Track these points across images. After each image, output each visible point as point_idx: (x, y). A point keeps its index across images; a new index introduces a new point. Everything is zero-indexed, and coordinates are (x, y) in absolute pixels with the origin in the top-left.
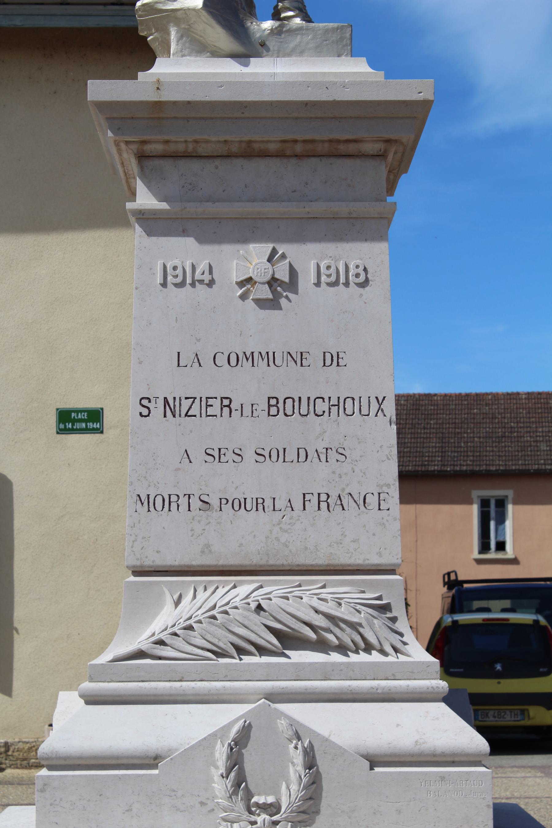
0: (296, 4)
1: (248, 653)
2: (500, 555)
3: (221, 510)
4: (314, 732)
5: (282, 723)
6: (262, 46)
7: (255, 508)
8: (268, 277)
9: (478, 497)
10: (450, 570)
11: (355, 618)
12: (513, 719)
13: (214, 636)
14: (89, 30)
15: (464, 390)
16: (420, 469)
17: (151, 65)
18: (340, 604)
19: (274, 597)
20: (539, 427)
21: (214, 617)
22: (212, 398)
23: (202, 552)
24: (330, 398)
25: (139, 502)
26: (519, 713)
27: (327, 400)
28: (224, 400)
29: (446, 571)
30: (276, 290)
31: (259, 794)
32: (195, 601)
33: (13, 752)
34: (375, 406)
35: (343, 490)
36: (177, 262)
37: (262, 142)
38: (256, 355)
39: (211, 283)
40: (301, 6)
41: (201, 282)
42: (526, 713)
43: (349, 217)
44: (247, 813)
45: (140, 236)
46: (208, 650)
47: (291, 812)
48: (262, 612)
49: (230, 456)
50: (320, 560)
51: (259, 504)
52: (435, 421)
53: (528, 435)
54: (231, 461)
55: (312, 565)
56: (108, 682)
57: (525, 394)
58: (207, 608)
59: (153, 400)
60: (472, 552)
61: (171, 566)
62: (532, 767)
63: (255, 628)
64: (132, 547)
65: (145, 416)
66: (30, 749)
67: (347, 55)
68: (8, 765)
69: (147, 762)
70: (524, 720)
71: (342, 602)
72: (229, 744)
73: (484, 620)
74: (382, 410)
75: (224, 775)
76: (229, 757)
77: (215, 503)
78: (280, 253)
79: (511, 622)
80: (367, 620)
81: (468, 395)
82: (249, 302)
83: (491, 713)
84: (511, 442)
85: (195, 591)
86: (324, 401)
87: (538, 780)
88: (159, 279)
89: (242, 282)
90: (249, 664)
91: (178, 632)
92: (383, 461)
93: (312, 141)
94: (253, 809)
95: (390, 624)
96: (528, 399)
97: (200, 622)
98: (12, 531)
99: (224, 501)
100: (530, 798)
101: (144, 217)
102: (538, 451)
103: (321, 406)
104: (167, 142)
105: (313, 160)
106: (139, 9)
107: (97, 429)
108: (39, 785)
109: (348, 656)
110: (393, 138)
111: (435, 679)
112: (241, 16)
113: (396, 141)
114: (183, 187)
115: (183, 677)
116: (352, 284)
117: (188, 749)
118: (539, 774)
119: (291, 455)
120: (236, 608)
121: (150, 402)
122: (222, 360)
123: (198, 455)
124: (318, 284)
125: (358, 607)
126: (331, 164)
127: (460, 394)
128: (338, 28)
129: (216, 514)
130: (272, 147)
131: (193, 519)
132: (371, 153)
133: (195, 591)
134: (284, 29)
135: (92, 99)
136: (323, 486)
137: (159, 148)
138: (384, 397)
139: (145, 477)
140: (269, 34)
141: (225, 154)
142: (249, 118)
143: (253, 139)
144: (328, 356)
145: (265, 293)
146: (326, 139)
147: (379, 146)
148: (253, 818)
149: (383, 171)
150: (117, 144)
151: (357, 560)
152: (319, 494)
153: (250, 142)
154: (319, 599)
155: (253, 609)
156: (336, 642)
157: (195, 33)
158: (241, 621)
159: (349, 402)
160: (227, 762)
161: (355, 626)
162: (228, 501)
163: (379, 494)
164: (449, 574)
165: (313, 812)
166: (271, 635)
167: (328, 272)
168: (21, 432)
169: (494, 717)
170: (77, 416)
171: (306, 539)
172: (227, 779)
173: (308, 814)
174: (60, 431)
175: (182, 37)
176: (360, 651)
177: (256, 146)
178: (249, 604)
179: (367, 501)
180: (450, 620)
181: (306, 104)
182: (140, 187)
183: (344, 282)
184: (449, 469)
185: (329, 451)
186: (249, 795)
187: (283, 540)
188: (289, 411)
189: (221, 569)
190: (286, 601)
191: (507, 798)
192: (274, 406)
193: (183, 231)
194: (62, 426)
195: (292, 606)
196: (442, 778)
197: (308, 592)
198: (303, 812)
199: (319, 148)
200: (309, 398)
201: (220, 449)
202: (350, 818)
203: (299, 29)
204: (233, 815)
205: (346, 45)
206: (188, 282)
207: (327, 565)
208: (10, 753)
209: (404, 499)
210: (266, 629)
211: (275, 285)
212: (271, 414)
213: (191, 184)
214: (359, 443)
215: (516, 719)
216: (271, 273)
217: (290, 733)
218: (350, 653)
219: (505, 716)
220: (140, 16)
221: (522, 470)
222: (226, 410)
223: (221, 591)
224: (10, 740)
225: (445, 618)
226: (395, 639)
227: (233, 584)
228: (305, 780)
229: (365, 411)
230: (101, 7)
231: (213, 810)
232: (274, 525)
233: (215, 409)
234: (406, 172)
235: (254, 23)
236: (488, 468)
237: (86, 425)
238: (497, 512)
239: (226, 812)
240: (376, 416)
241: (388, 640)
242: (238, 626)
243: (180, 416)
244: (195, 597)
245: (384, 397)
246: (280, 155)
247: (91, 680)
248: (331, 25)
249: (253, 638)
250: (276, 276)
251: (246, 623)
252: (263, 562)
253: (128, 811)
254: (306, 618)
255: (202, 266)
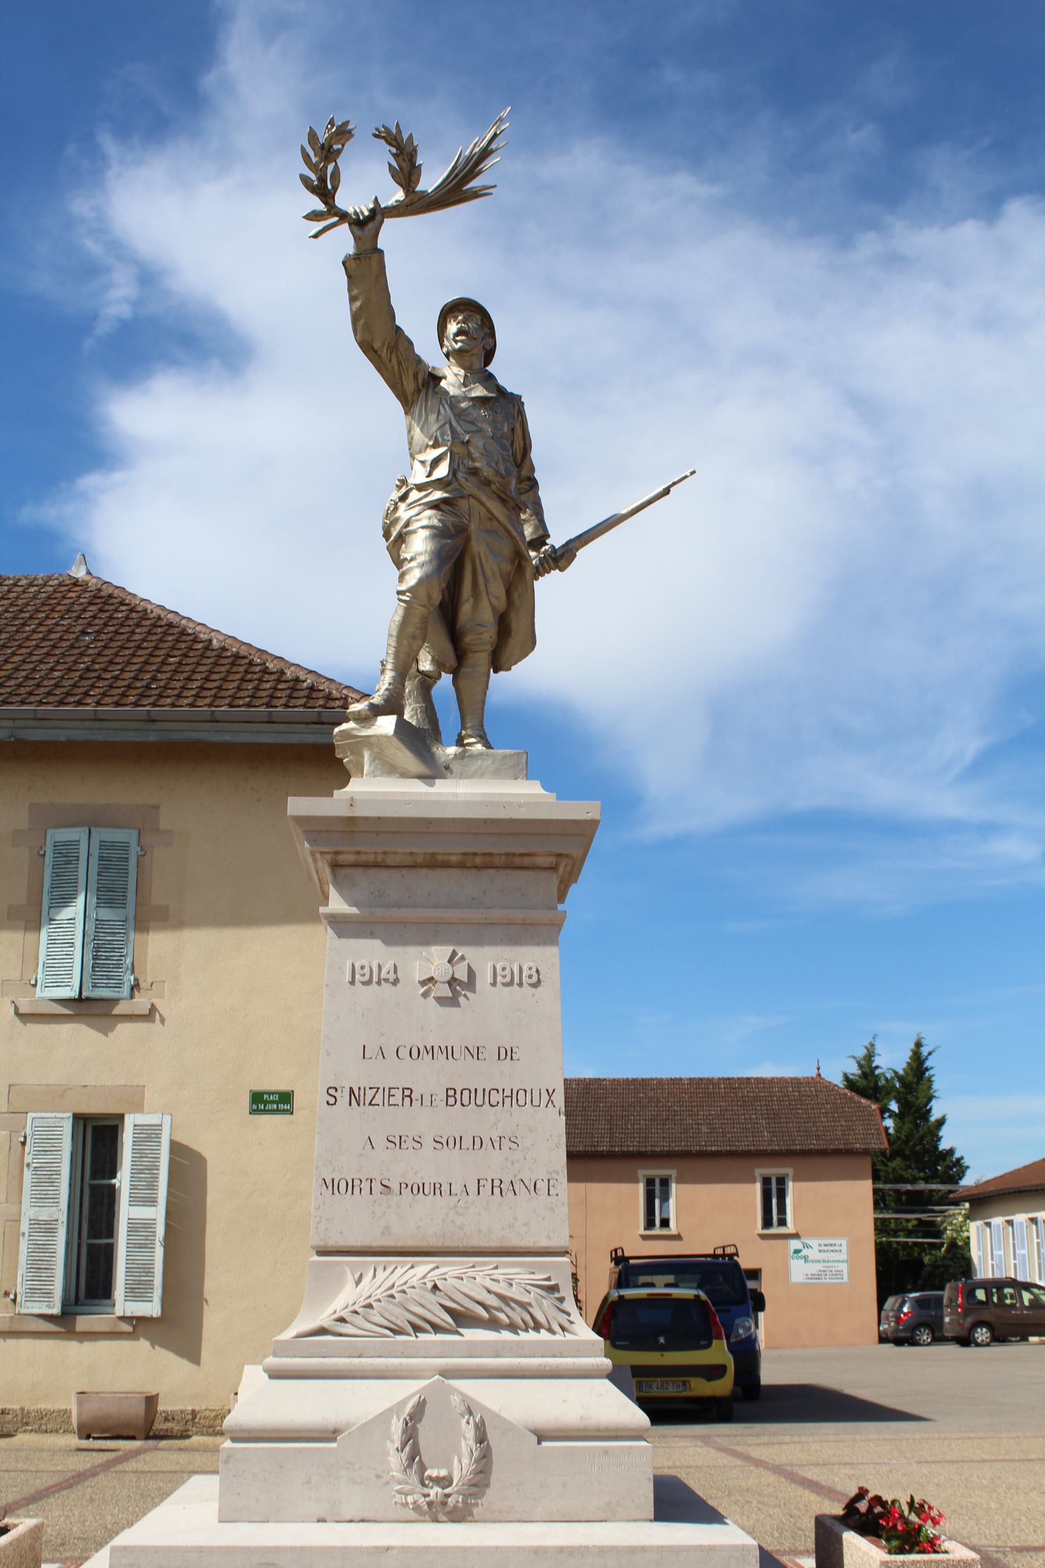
0: (477, 732)
1: (424, 1331)
2: (664, 1232)
3: (401, 1193)
4: (486, 1408)
5: (455, 1399)
6: (446, 768)
7: (432, 1193)
8: (448, 977)
9: (644, 1176)
10: (617, 1247)
11: (525, 1298)
12: (675, 1390)
13: (392, 1315)
14: (292, 745)
15: (631, 1075)
16: (590, 1149)
17: (345, 784)
18: (511, 1285)
19: (450, 1277)
20: (701, 1111)
21: (392, 1296)
22: (394, 1088)
23: (383, 1234)
24: (503, 1090)
25: (324, 1185)
26: (681, 1384)
27: (501, 1092)
28: (405, 1090)
29: (613, 1248)
30: (455, 988)
31: (433, 1468)
32: (375, 1280)
33: (200, 1419)
34: (545, 1098)
35: (515, 1176)
36: (365, 962)
37: (445, 854)
38: (436, 1049)
39: (396, 982)
40: (482, 733)
41: (386, 980)
42: (688, 1384)
43: (524, 924)
44: (421, 1486)
45: (332, 938)
46: (387, 1328)
47: (463, 1485)
48: (438, 1292)
49: (410, 1143)
50: (493, 1243)
51: (437, 1189)
52: (604, 1104)
53: (690, 1118)
54: (411, 1148)
55: (485, 1248)
56: (291, 1357)
57: (688, 1079)
58: (386, 1287)
59: (339, 1090)
60: (638, 1228)
61: (353, 1247)
62: (693, 1437)
63: (431, 1307)
64: (317, 1228)
65: (332, 1105)
66: (216, 1417)
67: (522, 778)
68: (195, 1432)
69: (326, 1435)
70: (686, 1391)
71: (513, 1283)
72: (405, 1419)
73: (648, 1295)
74: (552, 1102)
75: (399, 1449)
76: (404, 1432)
77: (395, 1187)
78: (460, 955)
79: (674, 1296)
80: (536, 1300)
81: (634, 1080)
82: (431, 1000)
83: (655, 1384)
84: (675, 1124)
85: (375, 1270)
86: (498, 1092)
87: (698, 1450)
88: (348, 977)
89: (424, 981)
90: (424, 1342)
91: (358, 1310)
92: (552, 1149)
93: (490, 854)
94: (427, 1482)
95: (558, 1304)
96: (690, 1084)
97: (379, 1300)
98: (205, 1206)
99: (404, 1186)
100: (691, 1467)
101: (336, 920)
102: (699, 1133)
103: (496, 1097)
104: (358, 853)
105: (492, 872)
106: (337, 735)
107: (287, 1110)
108: (222, 1456)
109: (518, 1334)
110: (565, 853)
111: (599, 1356)
112: (428, 742)
113: (566, 856)
114: (372, 893)
115: (362, 1354)
116: (525, 984)
117: (366, 1423)
118: (700, 1443)
119: (467, 1143)
120: (413, 1287)
121: (336, 1091)
122: (404, 1053)
123: (380, 1141)
124: (494, 984)
125: (528, 1288)
126: (507, 875)
127: (627, 1079)
128: (514, 755)
129: (395, 1198)
130: (454, 859)
131: (375, 1202)
132: (544, 865)
133: (375, 1270)
134: (467, 755)
135: (291, 814)
136: (496, 1173)
137: (351, 858)
138: (554, 1090)
139: (330, 1162)
140: (453, 758)
141: (411, 864)
142: (433, 833)
143: (435, 851)
144: (503, 1051)
145: (446, 992)
146: (503, 852)
147: (550, 860)
148: (426, 1491)
149: (554, 881)
150: (313, 854)
151: (528, 1242)
152: (493, 1180)
153: (433, 854)
154: (491, 1279)
155: (429, 1288)
156: (507, 1320)
157: (386, 757)
158: (418, 1300)
159: (522, 1093)
160: (402, 1436)
161: (524, 1306)
162: (407, 1185)
163: (549, 1180)
164: (616, 1250)
165: (483, 1486)
166: (446, 1314)
167: (503, 973)
168: (217, 1112)
169: (658, 1388)
170: (269, 1097)
171: (480, 1222)
172: (402, 1452)
173: (478, 1487)
174: (253, 1112)
175: (374, 760)
176: (530, 1330)
177: (439, 858)
178: (425, 1284)
179: (537, 1186)
180: (616, 1294)
181: (485, 821)
182: (333, 892)
183: (518, 982)
184: (616, 1150)
185: (503, 1139)
186: (423, 1468)
187: (458, 1223)
188: (466, 1101)
189: (400, 1250)
190: (460, 1281)
191: (669, 1468)
192: (451, 1096)
193: (371, 934)
194: (255, 1107)
195: (466, 1287)
196: (606, 1452)
197: (481, 1273)
198: (474, 1485)
199: (497, 861)
200: (484, 1090)
201: (400, 1137)
202: (518, 1490)
203: (480, 755)
204: (407, 1488)
205: (522, 769)
206: (374, 981)
207: (500, 1248)
208: (197, 1420)
209: (572, 1177)
210: (441, 1308)
211: (454, 984)
212: (449, 1104)
213: (379, 891)
214: (531, 1132)
215: (678, 1390)
216: (451, 973)
217: (463, 1408)
218: (519, 1331)
219: (668, 1388)
220: (337, 741)
221: (685, 1151)
222: (407, 1100)
223: (399, 1271)
224: (197, 1408)
225: (611, 1292)
226: (563, 1319)
227: (411, 1264)
228: (476, 1454)
229: (536, 1102)
230: (303, 726)
231: (388, 1483)
232: (450, 1209)
233: (397, 1099)
234: (576, 882)
235: (440, 749)
236: (653, 1149)
237: (278, 1107)
238: (661, 1191)
239: (400, 1484)
240: (547, 1106)
241: (556, 1319)
242: (416, 1305)
243: (364, 1104)
244: (374, 1276)
245: (554, 1090)
246: (461, 866)
247: (275, 1355)
248: (509, 751)
249: (429, 1316)
250: (456, 976)
251: (423, 1302)
252: (440, 1244)
253: (307, 1483)
254: (479, 1298)
255: (388, 966)
